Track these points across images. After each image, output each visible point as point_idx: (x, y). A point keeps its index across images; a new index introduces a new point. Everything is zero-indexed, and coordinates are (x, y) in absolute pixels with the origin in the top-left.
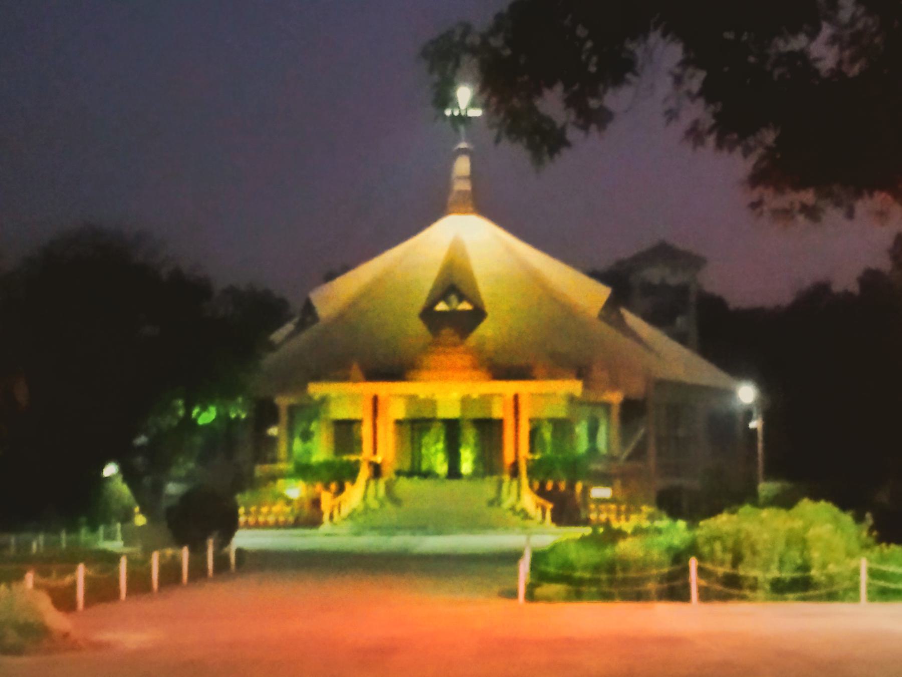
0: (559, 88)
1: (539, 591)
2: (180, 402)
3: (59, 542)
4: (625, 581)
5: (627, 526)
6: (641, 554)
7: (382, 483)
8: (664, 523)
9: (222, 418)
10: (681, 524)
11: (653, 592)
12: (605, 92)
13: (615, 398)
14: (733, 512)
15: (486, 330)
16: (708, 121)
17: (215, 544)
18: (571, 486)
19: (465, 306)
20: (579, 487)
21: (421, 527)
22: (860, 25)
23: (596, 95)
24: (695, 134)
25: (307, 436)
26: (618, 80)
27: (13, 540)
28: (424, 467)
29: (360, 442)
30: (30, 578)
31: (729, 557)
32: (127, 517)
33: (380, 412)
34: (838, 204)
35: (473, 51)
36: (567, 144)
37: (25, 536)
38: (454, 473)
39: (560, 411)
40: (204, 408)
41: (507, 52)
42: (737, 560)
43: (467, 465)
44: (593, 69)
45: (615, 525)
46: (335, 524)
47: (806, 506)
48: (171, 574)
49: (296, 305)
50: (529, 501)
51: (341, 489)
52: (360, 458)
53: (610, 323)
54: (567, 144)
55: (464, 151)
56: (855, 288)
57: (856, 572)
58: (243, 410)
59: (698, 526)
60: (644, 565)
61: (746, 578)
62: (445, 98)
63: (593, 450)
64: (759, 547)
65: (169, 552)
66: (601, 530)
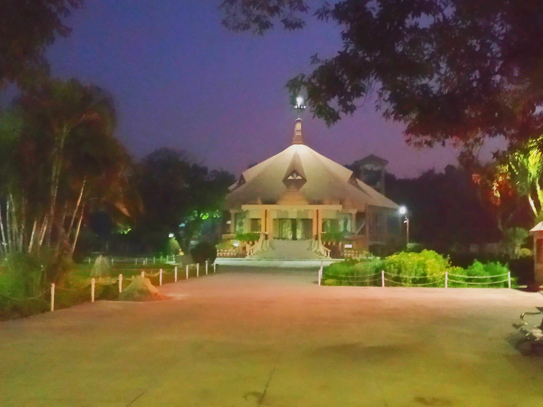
0: (336, 98)
1: (326, 281)
2: (196, 212)
3: (153, 261)
4: (358, 279)
5: (358, 259)
6: (363, 268)
7: (268, 241)
8: (372, 258)
9: (211, 217)
10: (378, 258)
11: (368, 283)
12: (354, 98)
13: (354, 212)
14: (398, 254)
15: (305, 186)
16: (391, 110)
17: (208, 263)
18: (337, 243)
19: (299, 177)
20: (340, 244)
21: (282, 258)
22: (448, 75)
23: (351, 100)
24: (386, 115)
25: (241, 224)
26: (358, 95)
27: (136, 260)
28: (284, 236)
29: (260, 227)
30: (143, 274)
31: (396, 270)
32: (177, 252)
33: (268, 215)
34: (439, 140)
35: (305, 84)
36: (339, 118)
37: (141, 259)
38: (294, 238)
39: (333, 216)
40: (205, 214)
41: (318, 85)
42: (399, 272)
43: (299, 236)
44: (349, 90)
45: (354, 258)
46: (251, 256)
47: (425, 252)
48: (193, 274)
49: (238, 177)
50: (322, 249)
51: (253, 244)
52: (260, 232)
53: (353, 184)
54: (339, 118)
55: (299, 121)
56: (444, 172)
57: (444, 276)
58: (219, 215)
59: (385, 259)
60: (365, 273)
61: (402, 278)
62: (294, 103)
63: (345, 230)
64: (408, 267)
65: (192, 265)
66: (349, 260)
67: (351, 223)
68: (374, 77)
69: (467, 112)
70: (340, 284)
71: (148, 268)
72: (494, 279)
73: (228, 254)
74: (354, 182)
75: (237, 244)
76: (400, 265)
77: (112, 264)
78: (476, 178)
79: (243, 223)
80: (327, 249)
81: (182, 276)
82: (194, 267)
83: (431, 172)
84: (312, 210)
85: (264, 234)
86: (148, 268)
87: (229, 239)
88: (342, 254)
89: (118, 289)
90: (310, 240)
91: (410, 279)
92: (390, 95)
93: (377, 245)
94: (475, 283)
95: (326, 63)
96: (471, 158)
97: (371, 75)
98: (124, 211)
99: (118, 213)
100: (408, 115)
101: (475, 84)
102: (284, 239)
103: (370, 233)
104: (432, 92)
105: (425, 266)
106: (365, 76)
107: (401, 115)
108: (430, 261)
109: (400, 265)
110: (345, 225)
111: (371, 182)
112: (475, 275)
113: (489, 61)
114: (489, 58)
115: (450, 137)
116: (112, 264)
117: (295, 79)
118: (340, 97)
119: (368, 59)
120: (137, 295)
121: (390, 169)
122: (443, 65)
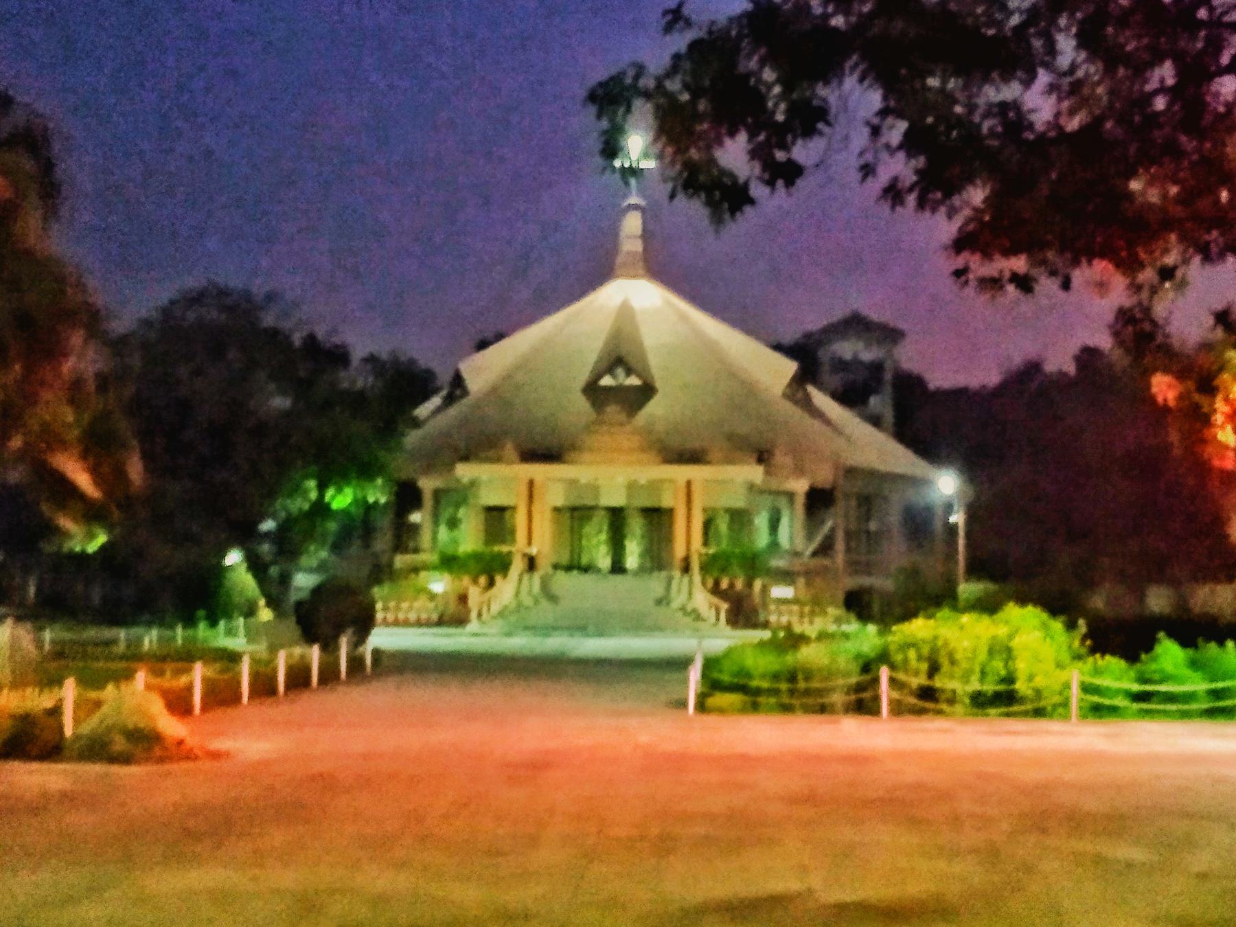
0: (742, 137)
4: (807, 692)
5: (811, 630)
8: (853, 626)
11: (839, 705)
12: (793, 143)
13: (800, 486)
15: (654, 408)
16: (909, 177)
18: (749, 584)
20: (758, 584)
21: (580, 628)
22: (1080, 73)
23: (785, 147)
25: (453, 524)
26: (809, 132)
27: (122, 634)
28: (584, 561)
29: (513, 532)
30: (141, 677)
31: (924, 666)
32: (250, 611)
33: (536, 497)
35: (647, 95)
36: (752, 202)
37: (136, 631)
38: (618, 568)
40: (339, 490)
41: (685, 97)
42: (934, 669)
43: (632, 560)
45: (797, 629)
46: (484, 623)
49: (444, 377)
50: (702, 600)
51: (491, 583)
53: (796, 403)
55: (636, 207)
56: (1071, 368)
57: (1067, 686)
59: (890, 631)
60: (829, 674)
61: (943, 691)
63: (774, 545)
65: (298, 651)
67: (792, 520)
68: (855, 77)
69: (1135, 185)
70: (755, 707)
71: (163, 659)
72: (1216, 694)
73: (401, 616)
74: (800, 395)
75: (439, 584)
76: (934, 651)
77: (47, 647)
78: (1164, 387)
79: (460, 521)
80: (716, 600)
81: (264, 687)
82: (302, 657)
83: (1033, 368)
84: (671, 481)
85: (525, 555)
86: (163, 659)
87: (416, 570)
88: (762, 618)
89: (61, 727)
90: (664, 574)
91: (965, 693)
92: (907, 134)
93: (868, 591)
94: (1161, 707)
95: (710, 32)
96: (1147, 327)
97: (847, 71)
98: (83, 480)
99: (65, 491)
100: (959, 192)
101: (1160, 104)
102: (586, 569)
103: (848, 550)
104: (1031, 126)
105: (1008, 653)
106: (829, 71)
107: (939, 195)
108: (1024, 637)
109: (934, 651)
110: (774, 525)
111: (851, 397)
112: (1161, 682)
113: (1203, 33)
114: (1202, 24)
115: (1084, 260)
116: (47, 647)
117: (617, 79)
118: (752, 136)
119: (838, 21)
120: (120, 744)
121: (908, 357)
122: (1066, 46)
